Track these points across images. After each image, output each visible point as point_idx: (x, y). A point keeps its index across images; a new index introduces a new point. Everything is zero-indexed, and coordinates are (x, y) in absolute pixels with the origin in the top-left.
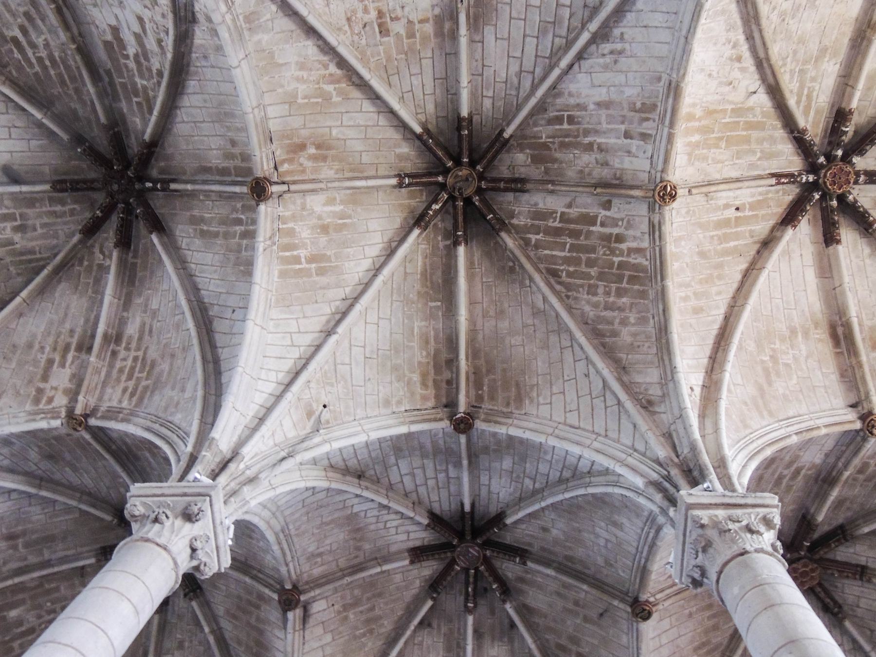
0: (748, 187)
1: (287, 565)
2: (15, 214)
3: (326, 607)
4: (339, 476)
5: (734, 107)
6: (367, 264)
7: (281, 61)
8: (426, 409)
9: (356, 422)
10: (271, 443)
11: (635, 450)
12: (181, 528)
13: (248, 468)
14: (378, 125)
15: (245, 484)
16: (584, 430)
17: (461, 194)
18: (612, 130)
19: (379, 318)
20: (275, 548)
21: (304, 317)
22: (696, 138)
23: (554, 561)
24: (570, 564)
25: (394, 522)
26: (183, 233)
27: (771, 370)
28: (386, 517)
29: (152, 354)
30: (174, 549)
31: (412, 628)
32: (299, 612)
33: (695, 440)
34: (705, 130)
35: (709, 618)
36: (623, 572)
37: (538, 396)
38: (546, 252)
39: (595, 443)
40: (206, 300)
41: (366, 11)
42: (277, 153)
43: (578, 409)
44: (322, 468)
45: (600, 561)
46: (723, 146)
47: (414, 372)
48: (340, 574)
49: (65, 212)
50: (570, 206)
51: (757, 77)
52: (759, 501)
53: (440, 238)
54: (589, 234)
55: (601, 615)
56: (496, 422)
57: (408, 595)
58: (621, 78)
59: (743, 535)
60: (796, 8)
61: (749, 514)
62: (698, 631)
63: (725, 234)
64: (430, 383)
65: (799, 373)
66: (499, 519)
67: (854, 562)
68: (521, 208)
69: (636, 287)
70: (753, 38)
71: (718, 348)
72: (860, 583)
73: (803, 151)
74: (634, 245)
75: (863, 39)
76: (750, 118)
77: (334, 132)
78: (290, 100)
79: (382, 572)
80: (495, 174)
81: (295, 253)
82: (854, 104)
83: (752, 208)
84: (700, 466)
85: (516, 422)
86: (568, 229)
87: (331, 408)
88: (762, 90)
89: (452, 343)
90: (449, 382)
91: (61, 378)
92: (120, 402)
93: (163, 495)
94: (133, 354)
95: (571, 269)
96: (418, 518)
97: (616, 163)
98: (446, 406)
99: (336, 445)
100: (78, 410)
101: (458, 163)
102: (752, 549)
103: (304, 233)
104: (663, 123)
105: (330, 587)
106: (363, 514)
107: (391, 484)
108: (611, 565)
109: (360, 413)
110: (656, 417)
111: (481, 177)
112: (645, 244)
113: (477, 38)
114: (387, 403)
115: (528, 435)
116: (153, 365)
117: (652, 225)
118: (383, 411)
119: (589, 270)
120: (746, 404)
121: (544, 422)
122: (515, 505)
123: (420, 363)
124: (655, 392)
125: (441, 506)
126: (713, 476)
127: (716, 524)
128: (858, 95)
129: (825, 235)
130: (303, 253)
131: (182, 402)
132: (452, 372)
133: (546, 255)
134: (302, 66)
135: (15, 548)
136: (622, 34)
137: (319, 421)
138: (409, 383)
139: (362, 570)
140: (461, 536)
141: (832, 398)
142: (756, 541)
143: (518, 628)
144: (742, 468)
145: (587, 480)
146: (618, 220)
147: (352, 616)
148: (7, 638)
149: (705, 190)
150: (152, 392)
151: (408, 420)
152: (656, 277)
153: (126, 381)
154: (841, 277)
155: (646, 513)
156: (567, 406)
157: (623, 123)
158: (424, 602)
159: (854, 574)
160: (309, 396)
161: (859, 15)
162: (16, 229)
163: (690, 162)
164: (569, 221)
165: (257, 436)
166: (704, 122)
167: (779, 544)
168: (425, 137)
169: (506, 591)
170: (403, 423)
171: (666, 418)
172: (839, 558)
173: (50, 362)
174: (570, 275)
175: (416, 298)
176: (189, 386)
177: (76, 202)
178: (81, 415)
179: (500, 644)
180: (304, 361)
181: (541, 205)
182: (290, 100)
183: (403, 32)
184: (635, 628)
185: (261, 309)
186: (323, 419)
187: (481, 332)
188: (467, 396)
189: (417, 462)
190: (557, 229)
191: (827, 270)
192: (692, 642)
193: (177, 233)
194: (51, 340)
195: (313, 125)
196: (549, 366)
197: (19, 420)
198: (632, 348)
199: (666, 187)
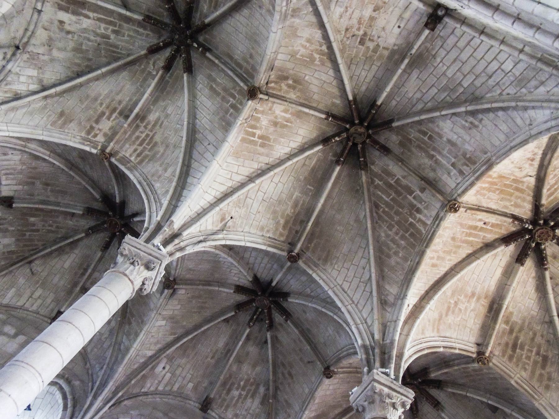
1: (176, 270)
2: (117, 23)
6: (287, 150)
7: (299, 35)
8: (279, 241)
9: (242, 233)
12: (142, 272)
14: (331, 84)
16: (348, 295)
17: (354, 140)
19: (279, 181)
21: (243, 166)
23: (301, 327)
26: (201, 80)
27: (451, 309)
29: (157, 138)
30: (135, 283)
31: (219, 320)
32: (171, 291)
33: (395, 340)
36: (330, 352)
40: (197, 127)
41: (359, 29)
42: (272, 77)
43: (351, 282)
45: (322, 340)
48: (198, 282)
49: (144, 34)
50: (404, 177)
52: (405, 393)
53: (331, 154)
55: (309, 362)
58: (467, 138)
59: (390, 407)
65: (463, 316)
66: (286, 295)
67: (435, 397)
68: (380, 162)
69: (412, 240)
74: (424, 219)
76: (520, 186)
77: (307, 78)
78: (293, 55)
80: (376, 137)
81: (254, 131)
85: (318, 271)
89: (309, 211)
90: (297, 232)
91: (106, 125)
92: (131, 155)
93: (139, 249)
94: (147, 132)
95: (386, 209)
98: (289, 244)
100: (108, 150)
101: (361, 124)
103: (264, 121)
104: (474, 175)
108: (326, 345)
109: (247, 229)
111: (369, 136)
112: (429, 222)
113: (408, 71)
114: (262, 229)
116: (156, 144)
117: (437, 216)
119: (394, 216)
120: (429, 321)
121: (332, 279)
123: (288, 215)
124: (391, 299)
126: (393, 366)
127: (381, 394)
129: (519, 256)
130: (258, 132)
131: (163, 178)
133: (378, 195)
134: (308, 41)
135: (46, 190)
136: (482, 119)
137: (225, 225)
139: (210, 285)
141: (471, 336)
146: (424, 201)
147: (194, 302)
148: (25, 229)
150: (150, 160)
151: (268, 243)
152: (424, 243)
153: (138, 145)
154: (512, 282)
157: (455, 158)
158: (231, 311)
162: (114, 32)
163: (475, 195)
164: (400, 186)
166: (495, 180)
168: (352, 103)
169: (271, 326)
170: (265, 245)
171: (388, 316)
172: (431, 393)
173: (103, 114)
174: (384, 212)
175: (303, 179)
176: (170, 170)
177: (151, 30)
178: (108, 154)
181: (390, 167)
182: (293, 55)
183: (371, 48)
185: (224, 156)
186: (228, 225)
188: (302, 245)
191: (508, 273)
192: (343, 393)
193: (198, 78)
194: (108, 101)
195: (298, 70)
196: (349, 252)
197: (76, 140)
198: (392, 269)
199: (455, 204)
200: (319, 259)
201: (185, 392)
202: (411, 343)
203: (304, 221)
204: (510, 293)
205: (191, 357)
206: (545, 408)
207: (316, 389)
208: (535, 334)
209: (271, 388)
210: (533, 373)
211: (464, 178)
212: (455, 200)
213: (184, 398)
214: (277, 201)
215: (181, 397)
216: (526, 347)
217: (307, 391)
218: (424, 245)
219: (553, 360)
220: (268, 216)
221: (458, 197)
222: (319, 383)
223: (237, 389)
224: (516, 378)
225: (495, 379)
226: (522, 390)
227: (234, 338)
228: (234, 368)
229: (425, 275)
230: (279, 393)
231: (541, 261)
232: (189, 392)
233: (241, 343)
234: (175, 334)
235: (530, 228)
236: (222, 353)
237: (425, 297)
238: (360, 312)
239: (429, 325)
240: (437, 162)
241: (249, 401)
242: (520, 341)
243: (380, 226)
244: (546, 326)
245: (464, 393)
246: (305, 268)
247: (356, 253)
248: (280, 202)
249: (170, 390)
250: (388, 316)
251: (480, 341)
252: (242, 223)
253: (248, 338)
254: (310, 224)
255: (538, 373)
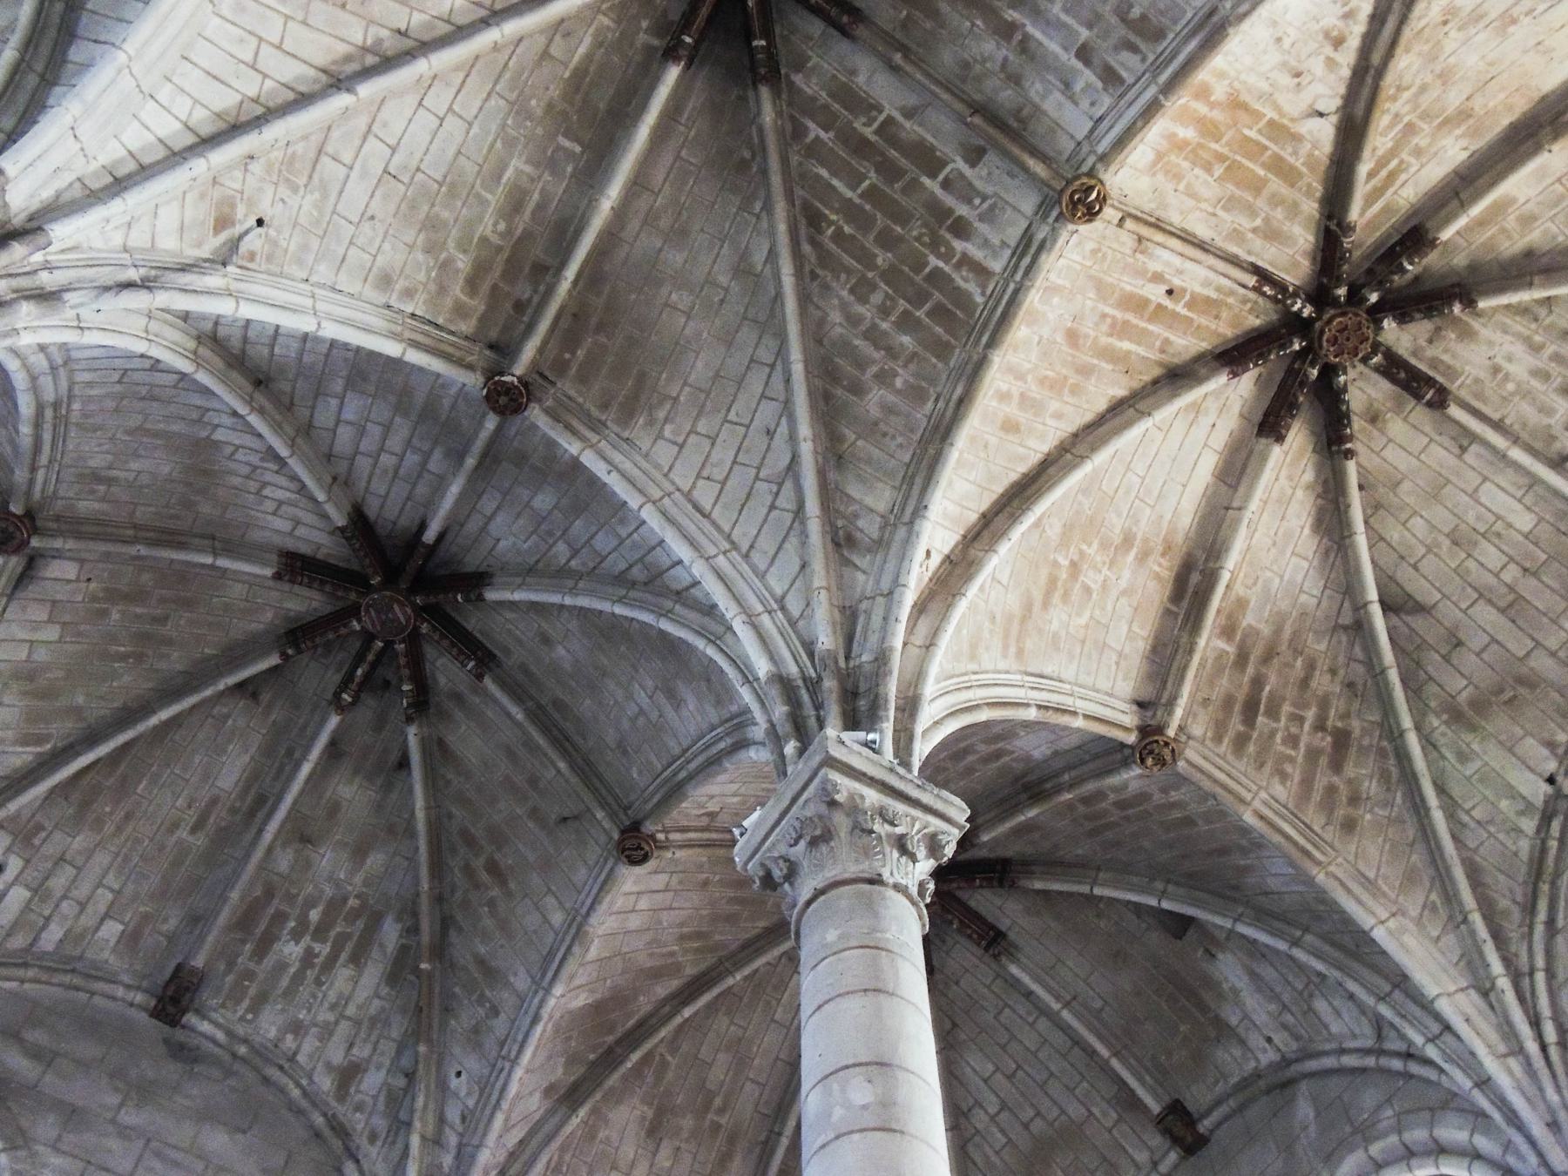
0: (1210, 268)
1: (33, 469)
3: (72, 576)
4: (220, 364)
5: (1276, 117)
8: (452, 333)
10: (117, 239)
11: (783, 608)
13: (48, 267)
15: (27, 298)
16: (714, 523)
18: (1065, 25)
19: (450, 109)
20: (26, 429)
21: (304, 23)
22: (1187, 133)
23: (532, 698)
24: (556, 716)
25: (279, 491)
27: (1060, 584)
28: (269, 477)
31: (221, 686)
33: (891, 649)
34: (1209, 130)
35: (731, 901)
36: (639, 775)
37: (666, 420)
38: (824, 173)
39: (721, 557)
43: (724, 483)
44: (195, 333)
45: (611, 737)
46: (1217, 174)
47: (465, 251)
48: (130, 532)
50: (909, 114)
51: (1342, 90)
52: (939, 806)
53: (644, 24)
54: (913, 186)
55: (565, 819)
56: (568, 427)
57: (243, 627)
59: (888, 849)
60: (1476, 17)
61: (914, 820)
62: (704, 912)
63: (1126, 323)
64: (485, 288)
65: (1097, 612)
66: (477, 581)
67: (990, 920)
69: (939, 330)
70: (1383, 22)
71: (1005, 506)
72: (980, 952)
73: (1324, 260)
75: (1531, 135)
79: (212, 567)
82: (1446, 234)
83: (1190, 305)
84: (877, 696)
86: (882, 154)
87: (272, 233)
88: (1334, 119)
89: (564, 235)
90: (519, 306)
95: (847, 229)
96: (330, 509)
97: (1035, 89)
98: (491, 347)
99: (248, 311)
102: (891, 881)
104: (1155, 77)
105: (103, 547)
106: (228, 450)
107: (310, 425)
108: (625, 753)
109: (323, 273)
110: (847, 571)
112: (997, 266)
114: (385, 281)
115: (614, 482)
118: (370, 293)
122: (518, 575)
124: (869, 527)
125: (382, 507)
126: (888, 727)
127: (854, 808)
128: (1462, 222)
129: (1266, 415)
132: (535, 291)
133: (818, 177)
137: (234, 245)
138: (445, 266)
139: (182, 546)
140: (391, 578)
142: (903, 871)
143: (410, 774)
144: (934, 728)
145: (668, 604)
146: (978, 193)
149: (1145, 231)
151: (407, 334)
152: (981, 334)
154: (1248, 497)
155: (734, 708)
156: (708, 467)
157: (1090, 26)
158: (265, 654)
159: (981, 937)
160: (237, 186)
161: (1553, 92)
163: (1152, 169)
164: (894, 142)
165: (97, 214)
166: (1217, 115)
167: (931, 886)
169: (422, 703)
170: (395, 336)
171: (862, 582)
172: (972, 904)
174: (839, 236)
175: (539, 112)
179: (365, 784)
180: (260, 110)
184: (608, 866)
186: (244, 247)
187: (626, 248)
188: (541, 350)
189: (382, 411)
190: (865, 142)
191: (1236, 471)
192: (681, 925)
199: (1091, 189)
200: (605, 407)
201: (89, 955)
202: (938, 681)
203: (547, 269)
204: (1243, 531)
205: (109, 828)
206: (1342, 884)
207: (592, 908)
208: (1311, 666)
209: (425, 925)
210: (1307, 783)
211: (1121, 96)
212: (1091, 174)
213: (88, 976)
214: (441, 185)
215: (73, 971)
216: (1287, 708)
217: (557, 918)
218: (985, 339)
219: (1366, 742)
220: (409, 237)
221: (1099, 166)
222: (605, 882)
223: (296, 936)
224: (1257, 804)
225: (1188, 821)
226: (1277, 838)
227: (279, 756)
228: (284, 861)
229: (982, 455)
230: (453, 937)
231: (1333, 438)
232: (106, 954)
233: (306, 769)
234: (39, 740)
235: (1306, 312)
236: (233, 811)
237: (978, 534)
238: (762, 576)
239: (991, 631)
240: (1026, 47)
241: (342, 976)
242: (1268, 688)
243: (826, 287)
244: (1344, 639)
245: (1085, 889)
246: (552, 434)
247: (740, 384)
248: (451, 186)
249: (28, 949)
250: (862, 582)
251: (1147, 693)
252: (305, 247)
253: (335, 750)
254: (571, 272)
255: (1322, 780)
